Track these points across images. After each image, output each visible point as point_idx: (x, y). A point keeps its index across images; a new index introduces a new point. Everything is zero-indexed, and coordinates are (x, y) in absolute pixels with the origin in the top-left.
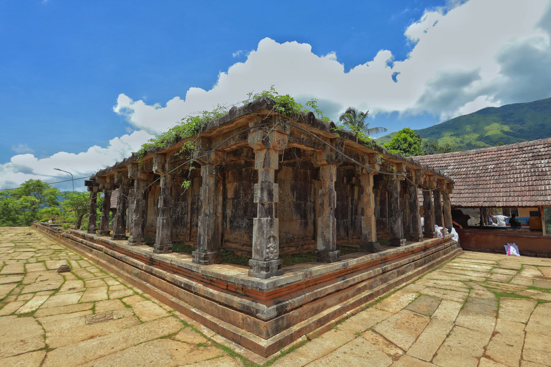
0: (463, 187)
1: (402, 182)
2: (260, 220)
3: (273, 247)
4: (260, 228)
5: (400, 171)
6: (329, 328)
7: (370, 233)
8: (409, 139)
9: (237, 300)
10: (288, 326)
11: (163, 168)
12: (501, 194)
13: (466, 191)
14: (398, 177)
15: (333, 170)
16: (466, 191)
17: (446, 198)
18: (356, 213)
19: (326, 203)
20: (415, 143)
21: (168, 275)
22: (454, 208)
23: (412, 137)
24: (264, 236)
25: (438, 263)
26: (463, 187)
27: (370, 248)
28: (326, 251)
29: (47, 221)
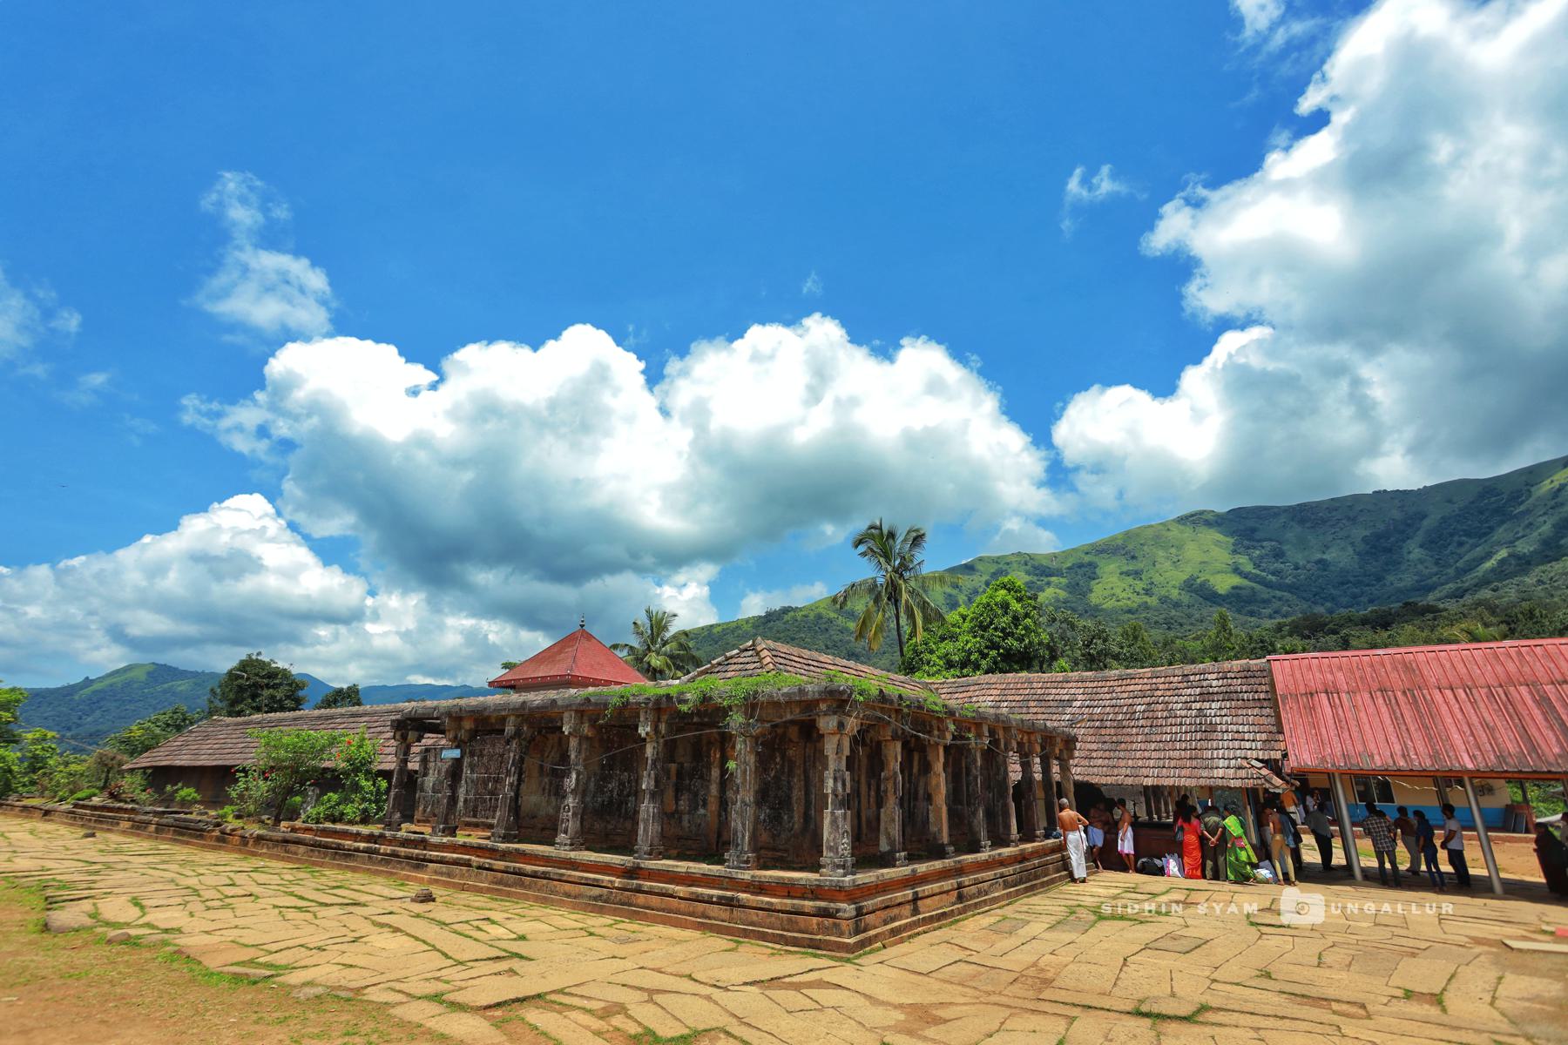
0: (1094, 746)
1: (982, 750)
2: (833, 813)
3: (845, 844)
4: (834, 822)
5: (979, 735)
6: (902, 941)
7: (940, 830)
8: (1016, 606)
9: (808, 905)
10: (865, 930)
11: (656, 729)
12: (1152, 763)
13: (1100, 754)
14: (978, 743)
15: (899, 745)
16: (1100, 754)
17: (1065, 769)
18: (916, 799)
19: (890, 786)
20: (1027, 615)
21: (681, 890)
22: (1078, 785)
23: (1019, 600)
24: (835, 831)
25: (1043, 885)
26: (1094, 746)
27: (940, 853)
28: (892, 852)
29: (89, 798)
